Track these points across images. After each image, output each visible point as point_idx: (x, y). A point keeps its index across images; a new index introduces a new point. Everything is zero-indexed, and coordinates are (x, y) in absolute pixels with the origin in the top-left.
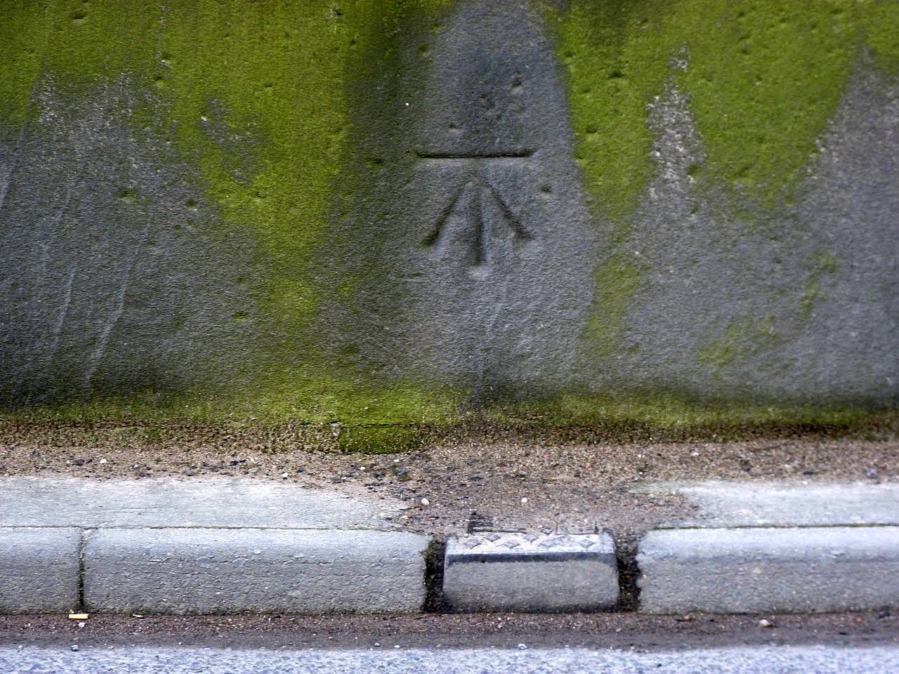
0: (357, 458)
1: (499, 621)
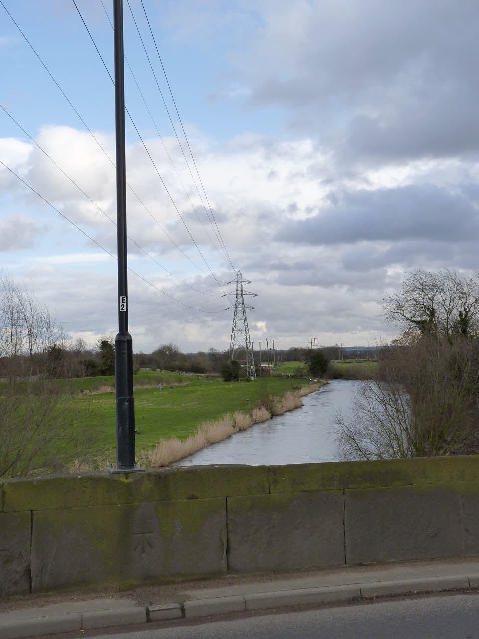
0: (122, 592)
1: (160, 622)
